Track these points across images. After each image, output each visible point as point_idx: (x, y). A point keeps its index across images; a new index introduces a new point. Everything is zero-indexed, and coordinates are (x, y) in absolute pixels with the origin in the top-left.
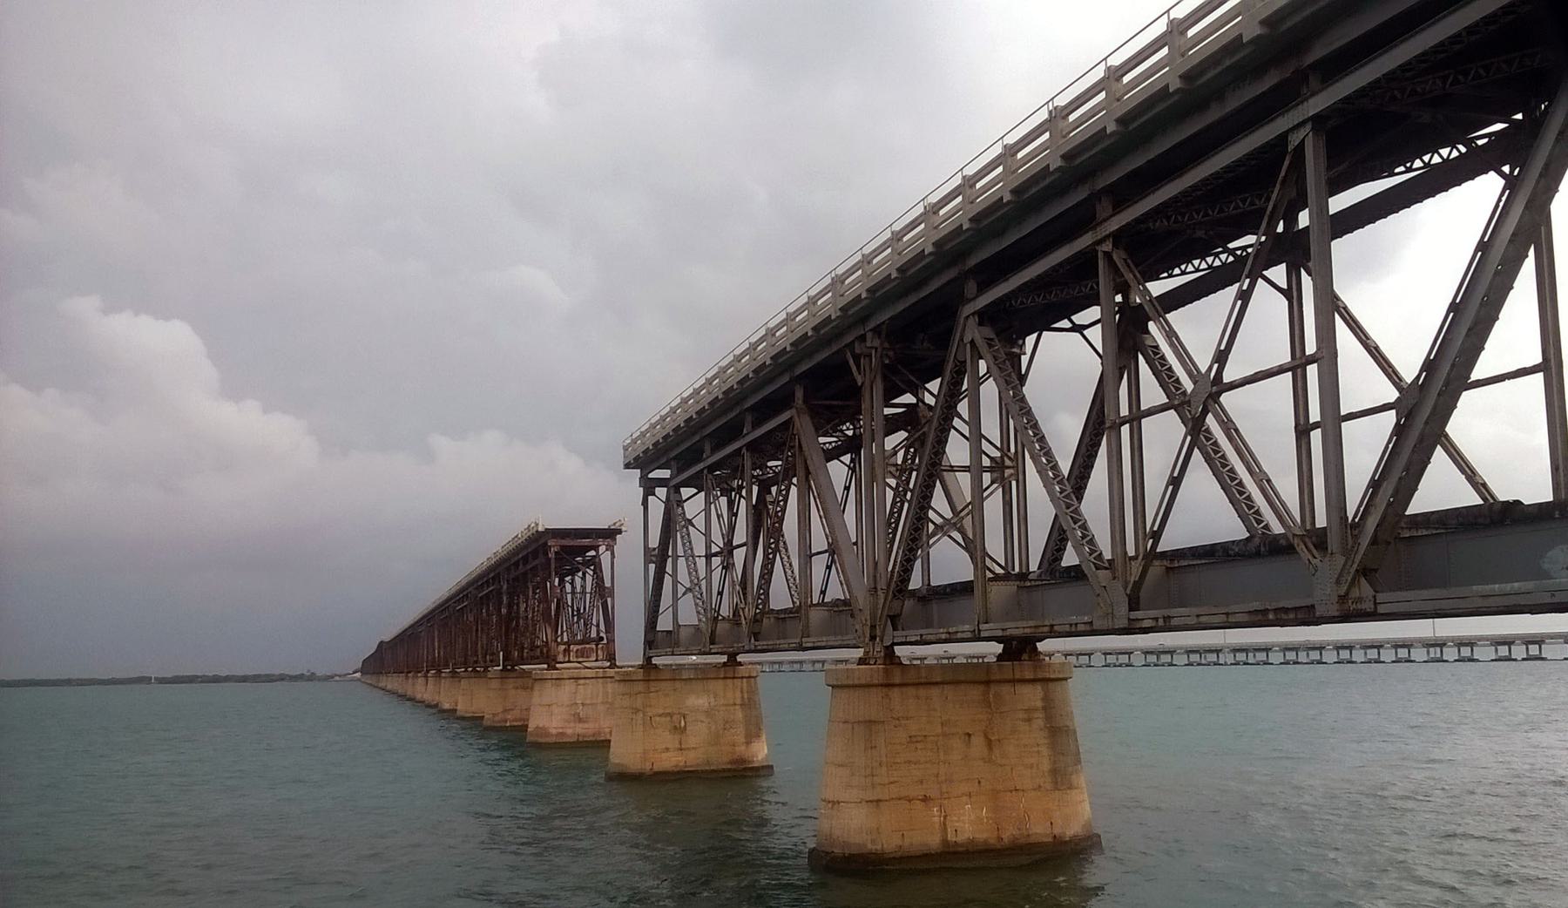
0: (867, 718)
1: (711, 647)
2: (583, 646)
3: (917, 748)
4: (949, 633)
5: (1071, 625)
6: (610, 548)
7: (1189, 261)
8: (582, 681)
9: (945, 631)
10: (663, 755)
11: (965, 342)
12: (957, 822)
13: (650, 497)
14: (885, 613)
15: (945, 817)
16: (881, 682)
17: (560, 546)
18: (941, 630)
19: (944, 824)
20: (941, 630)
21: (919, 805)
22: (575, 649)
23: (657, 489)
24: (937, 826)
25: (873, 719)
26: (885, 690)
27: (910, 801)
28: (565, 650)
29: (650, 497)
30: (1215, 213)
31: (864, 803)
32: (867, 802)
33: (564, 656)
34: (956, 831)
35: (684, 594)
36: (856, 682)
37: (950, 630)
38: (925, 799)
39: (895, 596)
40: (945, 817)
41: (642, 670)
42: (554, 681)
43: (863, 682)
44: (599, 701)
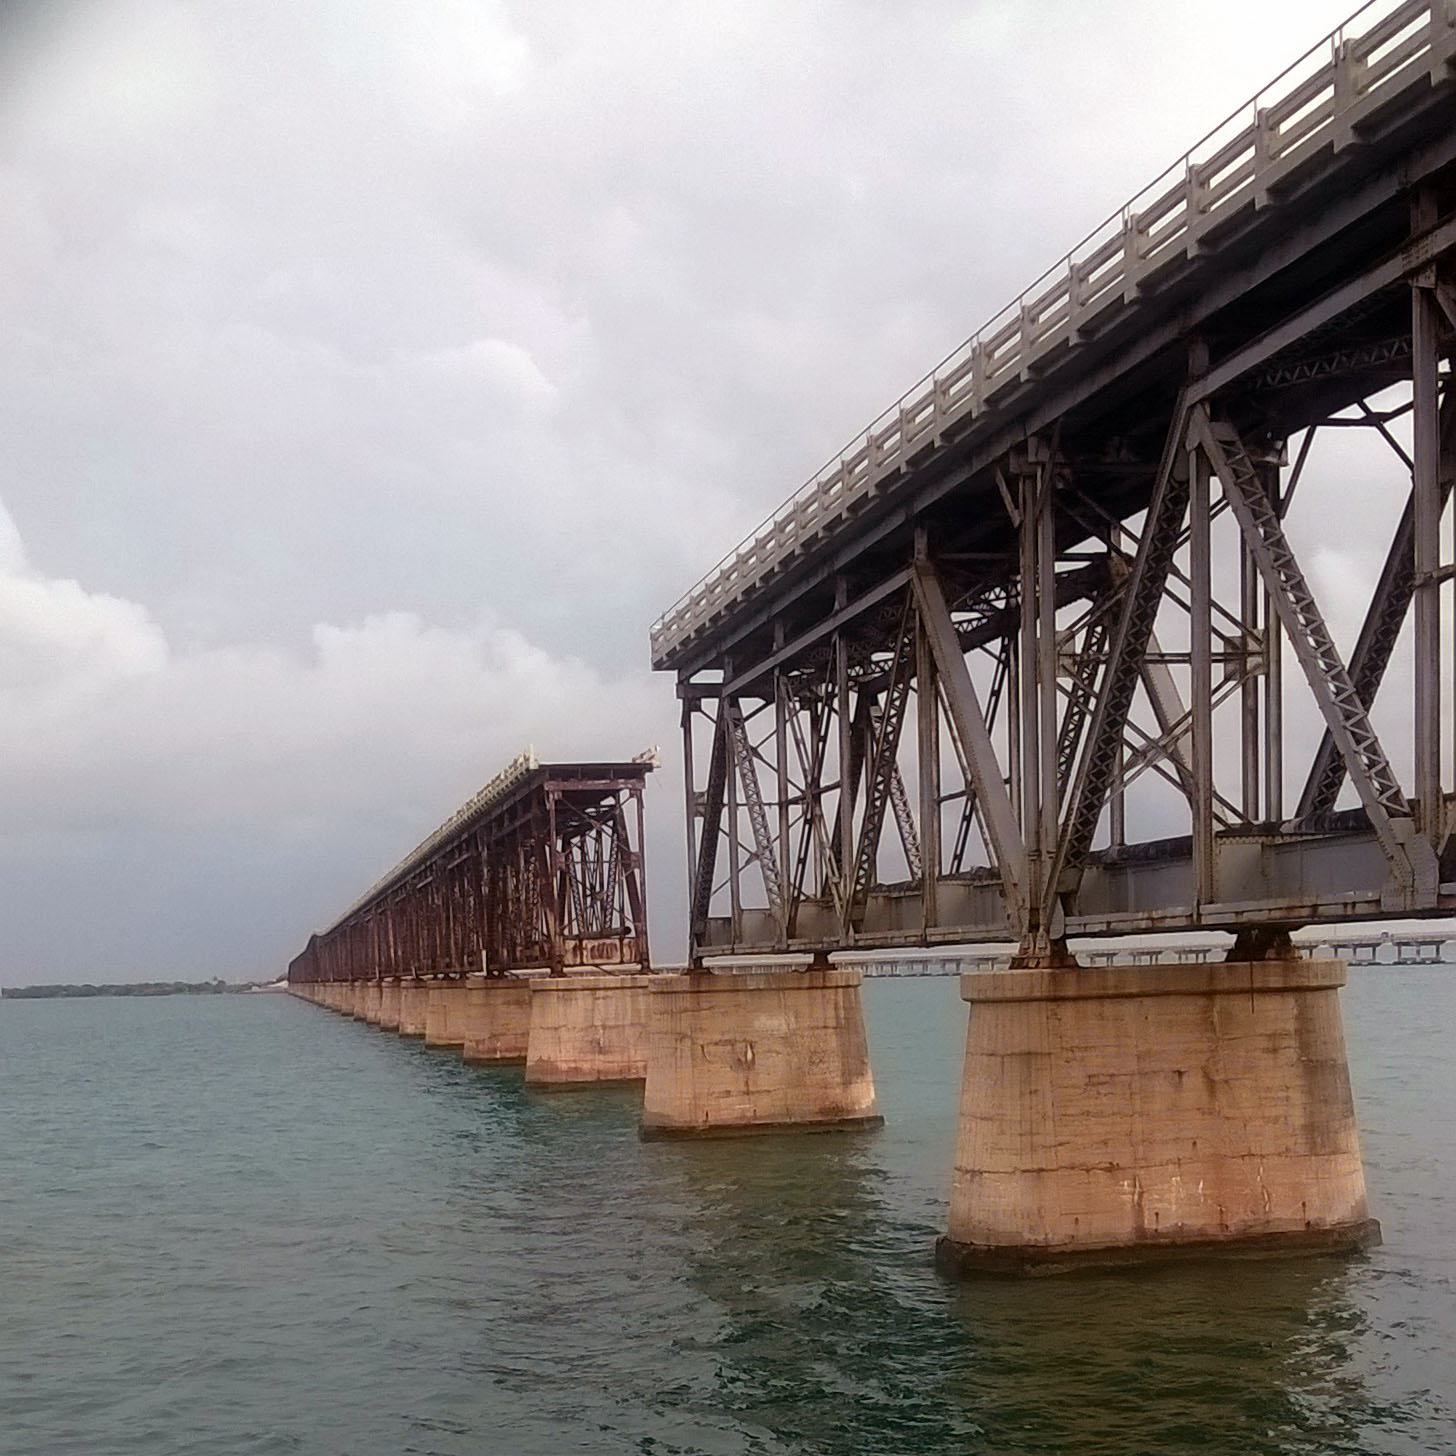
0: (1024, 1048)
1: (790, 942)
2: (601, 941)
3: (1099, 1093)
4: (1153, 919)
5: (1345, 905)
6: (636, 793)
8: (601, 993)
9: (1146, 915)
10: (721, 1100)
11: (1188, 448)
12: (1160, 1201)
13: (693, 714)
14: (1052, 892)
15: (1141, 1195)
16: (1046, 994)
17: (563, 791)
18: (1140, 915)
19: (1139, 1205)
20: (1140, 915)
21: (1103, 1177)
22: (589, 946)
23: (703, 700)
24: (1128, 1207)
25: (1033, 1050)
26: (1052, 1006)
27: (1088, 1171)
28: (575, 948)
29: (693, 714)
30: (1373, 358)
31: (1018, 1173)
32: (1024, 1171)
33: (575, 955)
34: (1157, 1214)
35: (748, 863)
36: (1009, 994)
37: (1155, 915)
38: (1111, 1168)
39: (1069, 862)
40: (1141, 1195)
41: (688, 977)
42: (561, 993)
43: (1018, 994)
44: (627, 1022)
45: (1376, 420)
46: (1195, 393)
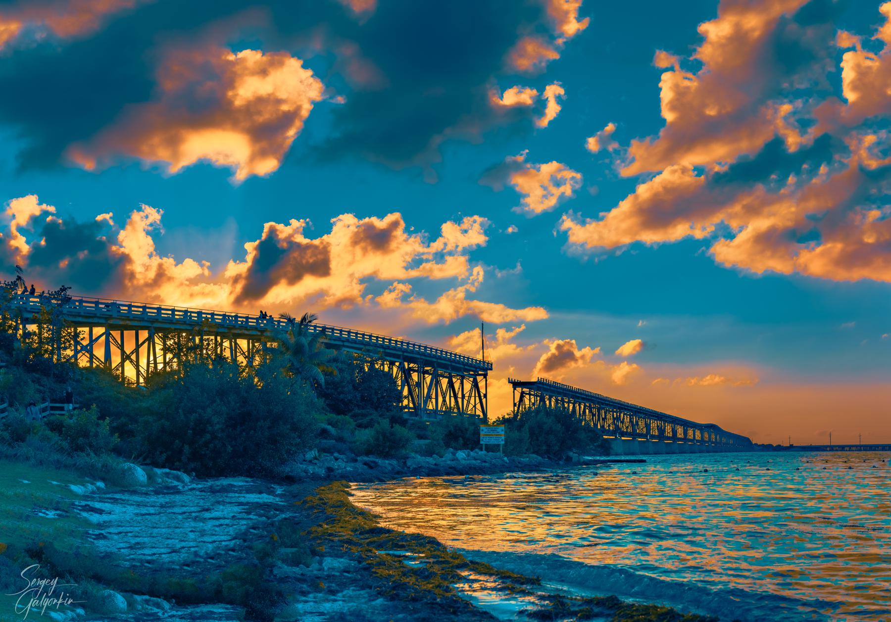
6: (485, 376)
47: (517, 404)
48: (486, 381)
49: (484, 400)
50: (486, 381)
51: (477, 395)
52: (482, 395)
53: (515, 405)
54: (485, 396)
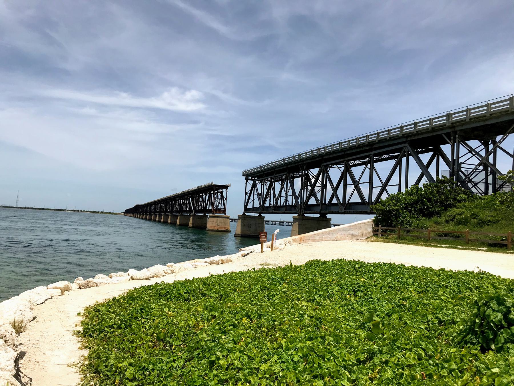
6: (227, 190)
7: (385, 158)
45: (339, 168)
46: (323, 164)
47: (249, 193)
48: (227, 192)
49: (225, 201)
50: (227, 192)
51: (222, 201)
52: (224, 198)
53: (246, 193)
54: (226, 199)
